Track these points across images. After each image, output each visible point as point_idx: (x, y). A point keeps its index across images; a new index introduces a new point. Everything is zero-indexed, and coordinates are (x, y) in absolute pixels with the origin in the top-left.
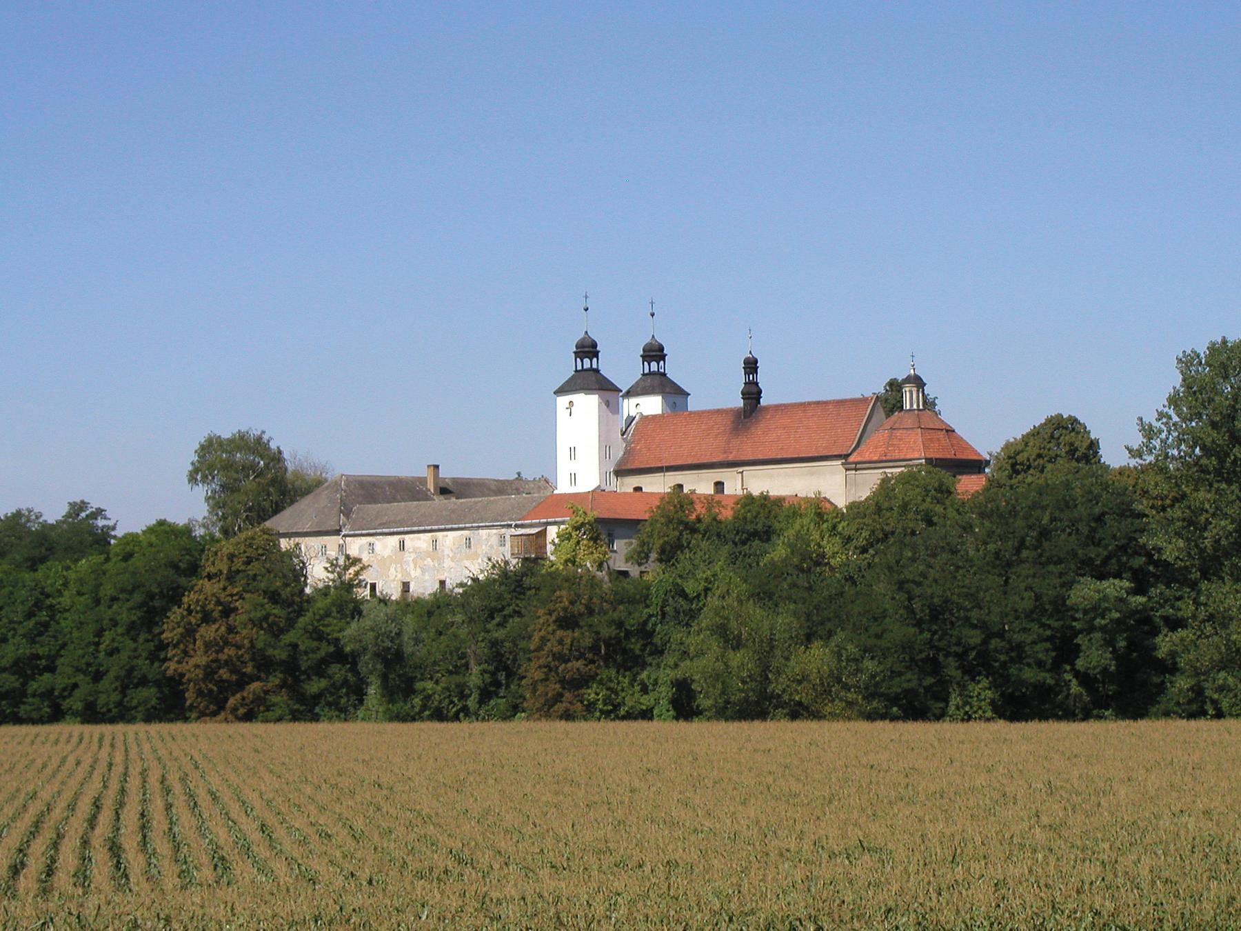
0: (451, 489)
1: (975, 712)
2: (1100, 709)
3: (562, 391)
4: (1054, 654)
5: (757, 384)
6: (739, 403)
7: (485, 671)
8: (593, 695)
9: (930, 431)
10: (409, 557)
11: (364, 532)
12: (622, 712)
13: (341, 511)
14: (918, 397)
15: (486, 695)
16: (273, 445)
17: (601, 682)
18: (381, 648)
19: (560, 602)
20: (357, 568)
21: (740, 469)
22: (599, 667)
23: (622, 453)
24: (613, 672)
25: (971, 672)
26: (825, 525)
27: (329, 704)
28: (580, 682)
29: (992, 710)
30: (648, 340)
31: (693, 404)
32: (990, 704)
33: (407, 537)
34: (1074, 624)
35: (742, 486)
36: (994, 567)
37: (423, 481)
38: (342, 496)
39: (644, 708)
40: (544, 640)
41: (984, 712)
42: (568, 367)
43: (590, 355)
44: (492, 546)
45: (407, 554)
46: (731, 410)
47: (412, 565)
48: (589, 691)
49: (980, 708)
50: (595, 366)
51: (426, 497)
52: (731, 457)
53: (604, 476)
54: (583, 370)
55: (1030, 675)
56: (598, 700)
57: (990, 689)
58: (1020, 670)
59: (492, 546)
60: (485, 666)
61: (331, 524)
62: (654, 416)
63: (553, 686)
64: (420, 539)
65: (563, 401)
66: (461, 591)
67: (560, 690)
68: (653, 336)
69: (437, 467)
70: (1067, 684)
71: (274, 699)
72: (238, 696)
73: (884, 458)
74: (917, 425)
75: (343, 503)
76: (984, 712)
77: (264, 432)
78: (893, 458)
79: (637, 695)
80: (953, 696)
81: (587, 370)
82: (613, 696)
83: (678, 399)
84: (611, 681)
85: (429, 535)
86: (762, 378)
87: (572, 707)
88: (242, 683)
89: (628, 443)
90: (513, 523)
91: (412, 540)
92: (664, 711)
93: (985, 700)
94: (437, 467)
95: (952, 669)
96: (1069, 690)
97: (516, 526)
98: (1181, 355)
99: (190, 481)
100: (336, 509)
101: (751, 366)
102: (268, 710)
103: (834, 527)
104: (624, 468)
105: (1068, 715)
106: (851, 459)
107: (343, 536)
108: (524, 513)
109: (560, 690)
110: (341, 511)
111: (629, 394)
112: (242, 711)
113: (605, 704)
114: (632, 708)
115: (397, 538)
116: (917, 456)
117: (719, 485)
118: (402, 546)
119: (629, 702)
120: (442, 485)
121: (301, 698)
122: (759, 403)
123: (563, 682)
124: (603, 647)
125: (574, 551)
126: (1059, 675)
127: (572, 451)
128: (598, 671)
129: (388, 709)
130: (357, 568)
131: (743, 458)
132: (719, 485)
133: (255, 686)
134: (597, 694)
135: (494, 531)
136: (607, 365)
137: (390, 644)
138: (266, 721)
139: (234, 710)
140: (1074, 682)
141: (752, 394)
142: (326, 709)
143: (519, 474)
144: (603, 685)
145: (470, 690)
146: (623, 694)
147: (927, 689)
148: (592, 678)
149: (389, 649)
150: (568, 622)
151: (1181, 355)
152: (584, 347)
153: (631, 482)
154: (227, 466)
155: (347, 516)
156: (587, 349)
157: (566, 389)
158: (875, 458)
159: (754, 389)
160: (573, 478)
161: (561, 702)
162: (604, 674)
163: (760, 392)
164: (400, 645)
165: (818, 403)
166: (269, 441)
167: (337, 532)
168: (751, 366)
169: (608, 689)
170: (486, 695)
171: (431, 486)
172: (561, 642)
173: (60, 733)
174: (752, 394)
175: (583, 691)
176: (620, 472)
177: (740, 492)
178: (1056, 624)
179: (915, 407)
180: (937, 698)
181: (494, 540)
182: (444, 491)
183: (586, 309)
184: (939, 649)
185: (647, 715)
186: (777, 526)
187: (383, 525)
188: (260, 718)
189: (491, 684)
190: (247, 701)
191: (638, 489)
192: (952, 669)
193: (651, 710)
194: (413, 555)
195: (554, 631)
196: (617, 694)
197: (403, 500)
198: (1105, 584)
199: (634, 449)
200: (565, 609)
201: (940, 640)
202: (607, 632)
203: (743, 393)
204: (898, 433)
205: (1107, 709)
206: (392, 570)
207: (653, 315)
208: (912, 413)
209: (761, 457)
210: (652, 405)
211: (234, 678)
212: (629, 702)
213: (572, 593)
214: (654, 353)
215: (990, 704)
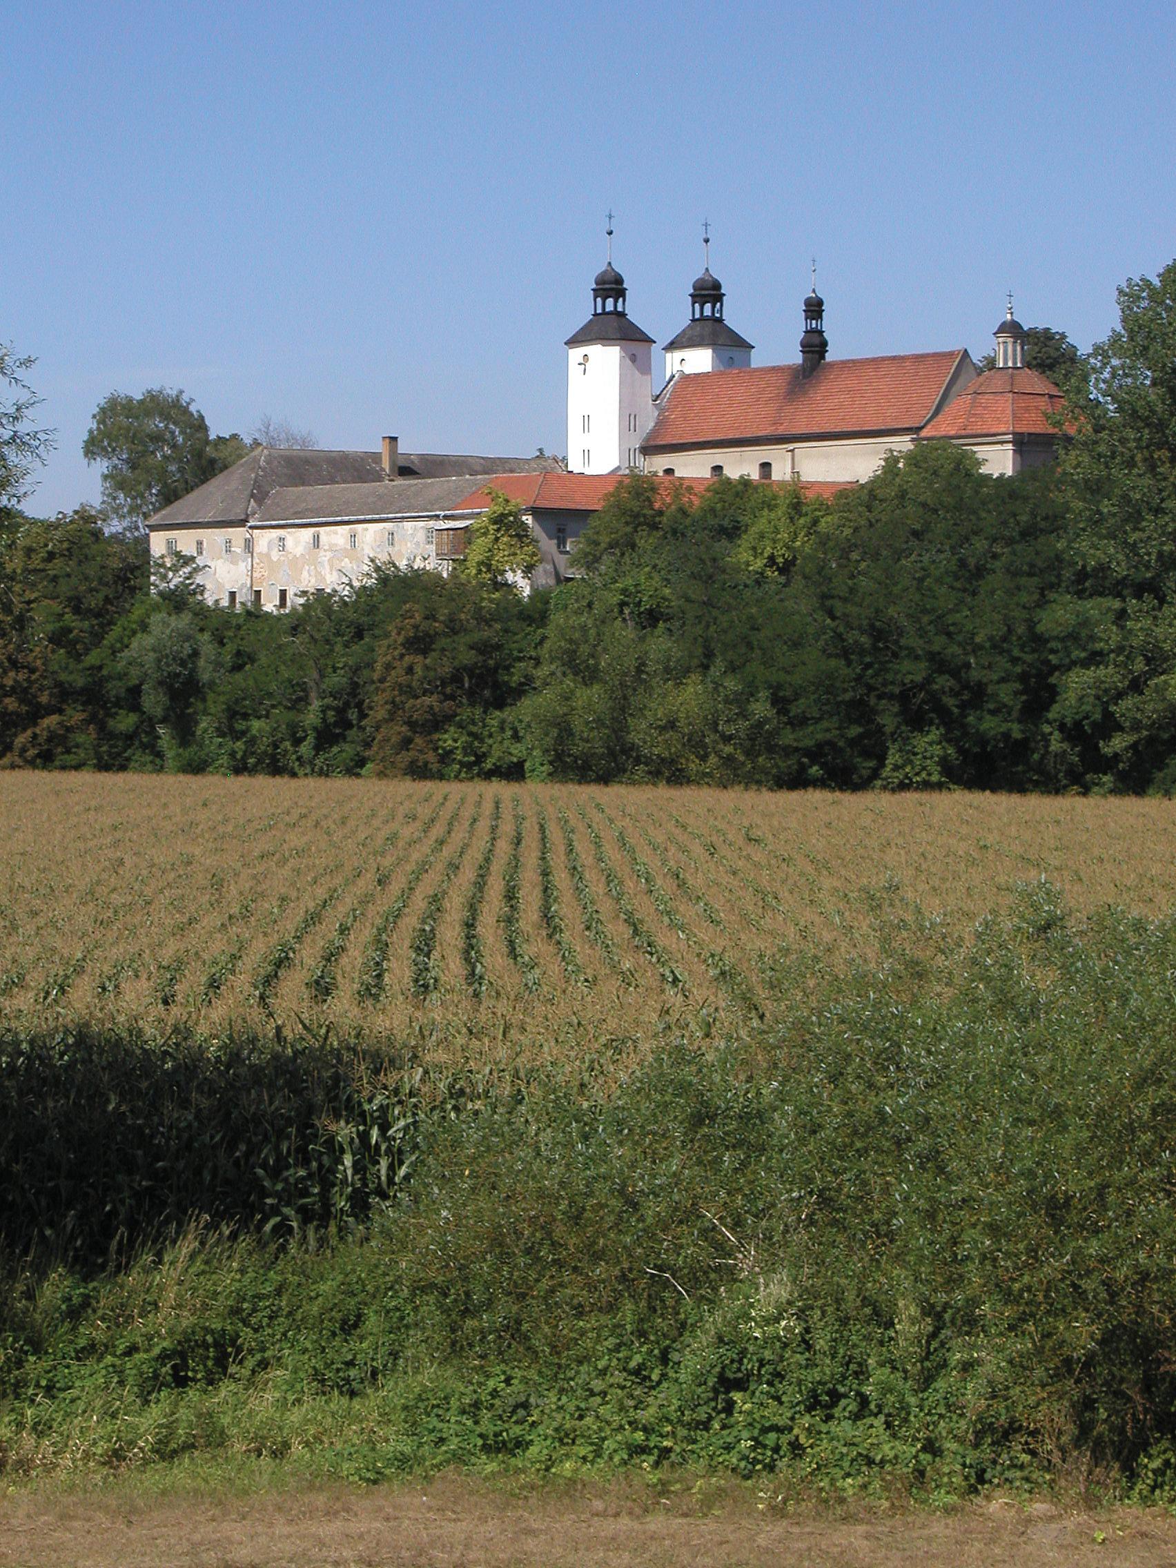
0: (415, 469)
1: (917, 774)
2: (1096, 772)
3: (574, 342)
4: (1024, 698)
5: (821, 332)
6: (795, 357)
7: (328, 707)
8: (450, 742)
9: (1026, 397)
10: (324, 556)
11: (274, 523)
12: (488, 765)
13: (252, 496)
14: (1014, 351)
15: (327, 737)
16: (193, 408)
17: (460, 726)
18: (165, 674)
19: (411, 618)
20: (187, 570)
21: (791, 446)
22: (460, 705)
23: (652, 424)
24: (478, 711)
25: (917, 722)
26: (802, 521)
27: (144, 746)
28: (436, 723)
29: (940, 773)
30: (603, 267)
31: (758, 359)
32: (938, 764)
33: (322, 530)
34: (1051, 657)
35: (793, 468)
36: (957, 578)
37: (376, 457)
38: (257, 474)
39: (515, 760)
40: (388, 667)
41: (929, 774)
42: (584, 308)
43: (613, 293)
44: (418, 544)
45: (322, 553)
46: (789, 367)
47: (327, 567)
48: (446, 736)
49: (924, 768)
50: (620, 309)
51: (380, 479)
53: (625, 452)
54: (604, 313)
55: (990, 725)
56: (457, 748)
57: (940, 743)
58: (980, 719)
59: (418, 544)
60: (329, 701)
61: (237, 513)
62: (706, 375)
63: (398, 728)
64: (336, 533)
65: (576, 354)
66: (302, 601)
67: (409, 734)
68: (707, 269)
69: (394, 439)
70: (1046, 739)
71: (81, 738)
72: (29, 732)
74: (1008, 388)
75: (257, 484)
76: (929, 774)
77: (181, 392)
79: (506, 743)
80: (891, 751)
81: (610, 313)
82: (476, 744)
83: (737, 353)
84: (474, 723)
85: (347, 527)
86: (830, 325)
87: (421, 757)
88: (36, 713)
89: (662, 410)
90: (442, 513)
91: (328, 534)
92: (537, 765)
93: (932, 757)
94: (394, 439)
95: (888, 720)
96: (1047, 746)
97: (446, 517)
98: (1124, 285)
99: (86, 455)
100: (248, 493)
101: (814, 309)
102: (68, 752)
103: (815, 522)
104: (652, 443)
105: (1050, 784)
106: (924, 433)
107: (251, 527)
108: (459, 500)
109: (409, 734)
110: (252, 496)
111: (673, 346)
112: (31, 753)
113: (465, 755)
114: (500, 759)
115: (312, 530)
116: (1003, 430)
117: (766, 467)
118: (316, 540)
119: (496, 753)
120: (402, 463)
121: (105, 734)
122: (823, 358)
123: (411, 724)
124: (466, 679)
125: (490, 550)
126: (1036, 726)
127: (586, 419)
128: (459, 711)
129: (179, 755)
130: (187, 570)
132: (766, 467)
133: (51, 721)
134: (455, 741)
135: (422, 524)
136: (636, 309)
137: (179, 669)
138: (63, 768)
139: (24, 750)
140: (1057, 735)
141: (815, 346)
142: (139, 753)
143: (541, 450)
144: (463, 728)
145: (304, 731)
146: (490, 741)
147: (853, 743)
148: (449, 718)
149: (178, 675)
150: (420, 643)
151: (1124, 285)
152: (604, 283)
153: (659, 463)
154: (133, 437)
155: (260, 502)
157: (580, 338)
159: (815, 339)
160: (586, 454)
161: (408, 750)
162: (465, 713)
163: (824, 344)
164: (193, 670)
165: (894, 358)
166: (188, 404)
167: (242, 523)
168: (814, 309)
169: (471, 734)
170: (327, 737)
171: (386, 465)
172: (410, 670)
174: (815, 346)
175: (436, 736)
176: (648, 450)
177: (788, 477)
178: (1029, 658)
179: (1010, 364)
180: (867, 755)
181: (421, 536)
182: (405, 471)
183: (707, 241)
184: (871, 688)
185: (515, 772)
186: (745, 519)
187: (297, 515)
188: (57, 763)
189: (336, 724)
190: (40, 740)
191: (669, 472)
192: (888, 720)
193: (520, 764)
194: (329, 554)
195: (402, 656)
196: (482, 741)
197: (344, 482)
198: (1089, 604)
199: (666, 418)
200: (416, 627)
201: (876, 675)
202: (468, 657)
203: (803, 345)
204: (983, 399)
205: (1105, 774)
206: (305, 574)
207: (707, 241)
208: (1005, 372)
209: (816, 430)
210: (700, 360)
211: (24, 708)
212: (496, 753)
215: (938, 764)
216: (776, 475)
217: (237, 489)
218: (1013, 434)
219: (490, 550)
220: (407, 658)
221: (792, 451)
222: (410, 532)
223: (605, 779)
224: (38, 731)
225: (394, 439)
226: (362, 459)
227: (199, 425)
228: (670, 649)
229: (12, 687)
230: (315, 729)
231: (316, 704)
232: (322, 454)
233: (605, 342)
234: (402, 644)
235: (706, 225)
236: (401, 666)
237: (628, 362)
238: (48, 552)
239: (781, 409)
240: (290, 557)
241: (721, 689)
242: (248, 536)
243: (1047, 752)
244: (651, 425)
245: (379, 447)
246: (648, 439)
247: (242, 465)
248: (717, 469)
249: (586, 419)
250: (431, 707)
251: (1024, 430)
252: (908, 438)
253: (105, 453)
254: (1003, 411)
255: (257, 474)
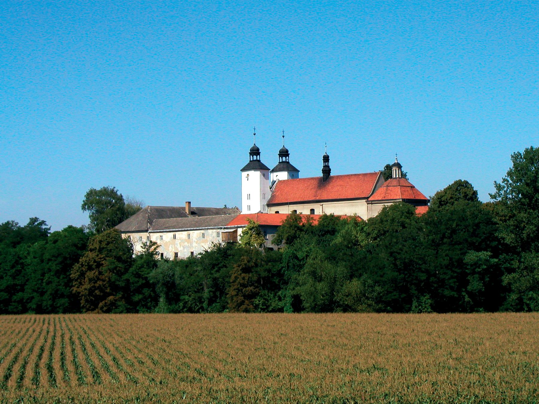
0: (196, 212)
3: (244, 170)
5: (329, 167)
6: (321, 175)
8: (257, 302)
9: (404, 187)
10: (177, 241)
13: (148, 222)
14: (399, 172)
15: (211, 301)
16: (119, 193)
17: (261, 296)
18: (165, 281)
19: (243, 261)
20: (155, 247)
21: (322, 204)
23: (270, 197)
25: (422, 292)
26: (358, 228)
27: (143, 306)
28: (252, 296)
30: (282, 147)
31: (301, 175)
32: (430, 305)
33: (177, 233)
35: (322, 211)
37: (184, 209)
38: (148, 215)
39: (280, 307)
40: (236, 278)
42: (246, 159)
44: (213, 237)
45: (177, 241)
46: (318, 178)
47: (179, 245)
48: (256, 300)
49: (426, 307)
50: (258, 159)
52: (317, 198)
54: (253, 160)
55: (447, 293)
56: (260, 304)
59: (213, 237)
60: (211, 289)
61: (144, 227)
63: (240, 298)
65: (244, 174)
69: (190, 203)
72: (103, 302)
73: (384, 199)
75: (149, 218)
77: (114, 188)
78: (388, 199)
81: (255, 161)
82: (266, 302)
83: (295, 173)
86: (331, 164)
87: (248, 307)
89: (273, 192)
90: (223, 227)
91: (179, 234)
96: (464, 299)
97: (224, 228)
99: (82, 209)
101: (326, 159)
103: (362, 229)
104: (271, 203)
106: (370, 199)
107: (150, 233)
110: (148, 222)
111: (273, 171)
112: (105, 309)
113: (263, 305)
114: (275, 307)
117: (312, 211)
118: (175, 237)
119: (273, 305)
120: (192, 210)
123: (245, 296)
124: (262, 281)
125: (249, 239)
127: (249, 196)
128: (260, 291)
129: (169, 308)
130: (155, 247)
131: (323, 199)
132: (312, 211)
133: (111, 298)
134: (259, 301)
137: (169, 280)
138: (116, 313)
140: (467, 296)
141: (327, 171)
142: (142, 308)
143: (225, 206)
144: (262, 297)
145: (204, 299)
146: (271, 301)
150: (246, 270)
151: (513, 154)
155: (151, 224)
156: (255, 151)
157: (246, 169)
158: (380, 199)
159: (327, 169)
160: (249, 207)
162: (262, 292)
163: (330, 170)
165: (355, 175)
166: (117, 191)
167: (146, 231)
168: (326, 159)
169: (264, 299)
170: (211, 301)
171: (187, 211)
172: (244, 279)
173: (26, 318)
174: (327, 171)
177: (321, 214)
179: (397, 176)
182: (193, 213)
183: (255, 134)
186: (337, 228)
187: (166, 228)
188: (113, 312)
190: (107, 304)
194: (180, 241)
195: (241, 274)
196: (268, 301)
197: (175, 217)
198: (480, 253)
200: (245, 264)
202: (264, 274)
203: (322, 171)
204: (390, 188)
206: (170, 247)
208: (396, 179)
209: (330, 198)
210: (283, 176)
211: (102, 294)
212: (273, 305)
213: (249, 257)
214: (284, 153)
215: (430, 305)
216: (316, 212)
217: (142, 220)
218: (402, 199)
219: (249, 239)
220: (242, 274)
221: (322, 205)
222: (211, 233)
223: (471, 311)
224: (106, 301)
225: (190, 203)
226: (179, 209)
227: (120, 198)
228: (344, 270)
229: (98, 287)
230: (208, 298)
231: (206, 290)
232: (166, 208)
233: (256, 170)
234: (241, 270)
235: (255, 129)
236: (240, 278)
237: (263, 177)
238: (107, 242)
239: (317, 191)
240: (165, 242)
241: (366, 283)
242: (148, 235)
243: (464, 301)
244: (270, 197)
245: (185, 205)
246: (269, 201)
247: (142, 212)
248: (296, 211)
249: (249, 196)
250: (251, 290)
251: (405, 198)
252: (365, 201)
253: (89, 208)
254: (397, 192)
255: (148, 215)
